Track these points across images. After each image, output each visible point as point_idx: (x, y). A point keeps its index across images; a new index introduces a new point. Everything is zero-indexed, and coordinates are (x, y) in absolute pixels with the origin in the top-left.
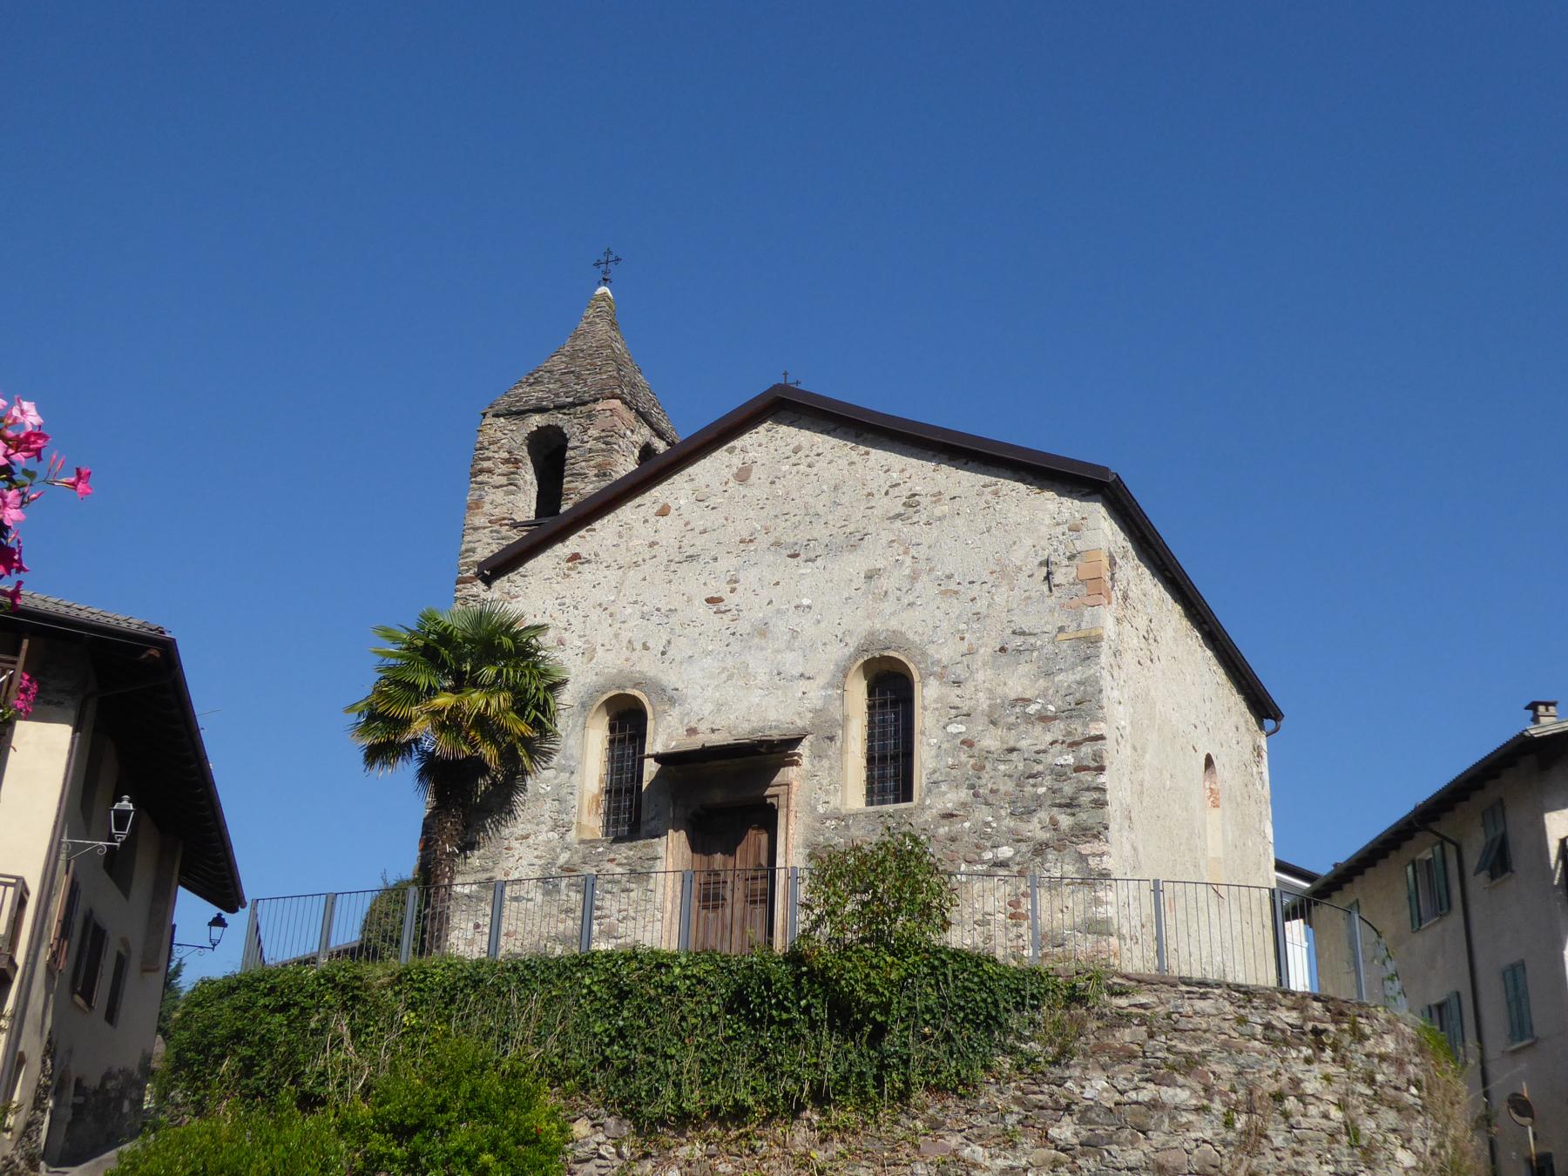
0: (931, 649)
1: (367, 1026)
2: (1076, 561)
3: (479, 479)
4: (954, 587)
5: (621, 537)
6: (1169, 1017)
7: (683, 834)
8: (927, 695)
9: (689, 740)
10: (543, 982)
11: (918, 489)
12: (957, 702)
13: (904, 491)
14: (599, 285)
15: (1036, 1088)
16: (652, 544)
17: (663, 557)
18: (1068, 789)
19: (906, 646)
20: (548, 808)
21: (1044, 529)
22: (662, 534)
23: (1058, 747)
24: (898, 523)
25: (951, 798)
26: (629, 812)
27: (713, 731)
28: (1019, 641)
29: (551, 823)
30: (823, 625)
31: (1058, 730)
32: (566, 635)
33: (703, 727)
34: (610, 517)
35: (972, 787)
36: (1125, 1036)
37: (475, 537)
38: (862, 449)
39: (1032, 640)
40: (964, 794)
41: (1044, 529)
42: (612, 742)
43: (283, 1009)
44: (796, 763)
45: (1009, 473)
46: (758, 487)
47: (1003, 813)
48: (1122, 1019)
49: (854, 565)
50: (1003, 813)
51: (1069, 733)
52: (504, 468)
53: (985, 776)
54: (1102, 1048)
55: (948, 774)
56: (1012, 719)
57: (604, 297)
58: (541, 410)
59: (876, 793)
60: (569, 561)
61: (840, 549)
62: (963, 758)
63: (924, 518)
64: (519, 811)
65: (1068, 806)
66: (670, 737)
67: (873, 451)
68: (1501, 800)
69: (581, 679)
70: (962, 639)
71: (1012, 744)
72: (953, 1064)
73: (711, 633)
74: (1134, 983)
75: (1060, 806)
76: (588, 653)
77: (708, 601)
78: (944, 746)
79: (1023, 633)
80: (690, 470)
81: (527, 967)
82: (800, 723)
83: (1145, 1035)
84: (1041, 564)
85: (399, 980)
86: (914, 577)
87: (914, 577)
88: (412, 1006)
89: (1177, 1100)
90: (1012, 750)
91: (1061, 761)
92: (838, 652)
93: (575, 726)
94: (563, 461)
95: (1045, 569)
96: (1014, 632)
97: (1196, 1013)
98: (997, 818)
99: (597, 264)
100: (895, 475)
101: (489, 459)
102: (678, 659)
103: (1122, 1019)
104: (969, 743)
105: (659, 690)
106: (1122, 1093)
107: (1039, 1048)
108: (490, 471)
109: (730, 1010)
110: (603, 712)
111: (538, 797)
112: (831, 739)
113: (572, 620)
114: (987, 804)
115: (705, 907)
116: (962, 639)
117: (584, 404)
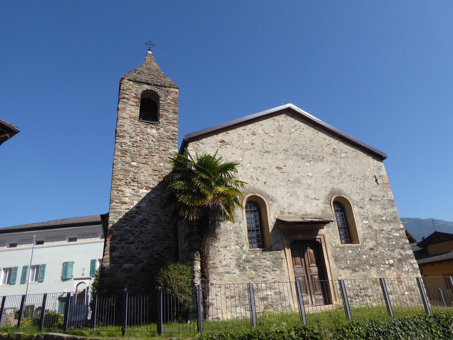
0: (352, 197)
2: (382, 178)
3: (124, 100)
11: (335, 147)
16: (252, 144)
24: (332, 156)
25: (371, 244)
27: (289, 213)
30: (317, 183)
33: (286, 211)
34: (234, 130)
52: (134, 100)
61: (317, 161)
62: (370, 231)
66: (275, 214)
67: (319, 132)
71: (381, 228)
77: (276, 167)
78: (364, 227)
80: (260, 122)
98: (386, 251)
99: (146, 44)
101: (127, 94)
102: (271, 186)
111: (227, 231)
117: (166, 87)
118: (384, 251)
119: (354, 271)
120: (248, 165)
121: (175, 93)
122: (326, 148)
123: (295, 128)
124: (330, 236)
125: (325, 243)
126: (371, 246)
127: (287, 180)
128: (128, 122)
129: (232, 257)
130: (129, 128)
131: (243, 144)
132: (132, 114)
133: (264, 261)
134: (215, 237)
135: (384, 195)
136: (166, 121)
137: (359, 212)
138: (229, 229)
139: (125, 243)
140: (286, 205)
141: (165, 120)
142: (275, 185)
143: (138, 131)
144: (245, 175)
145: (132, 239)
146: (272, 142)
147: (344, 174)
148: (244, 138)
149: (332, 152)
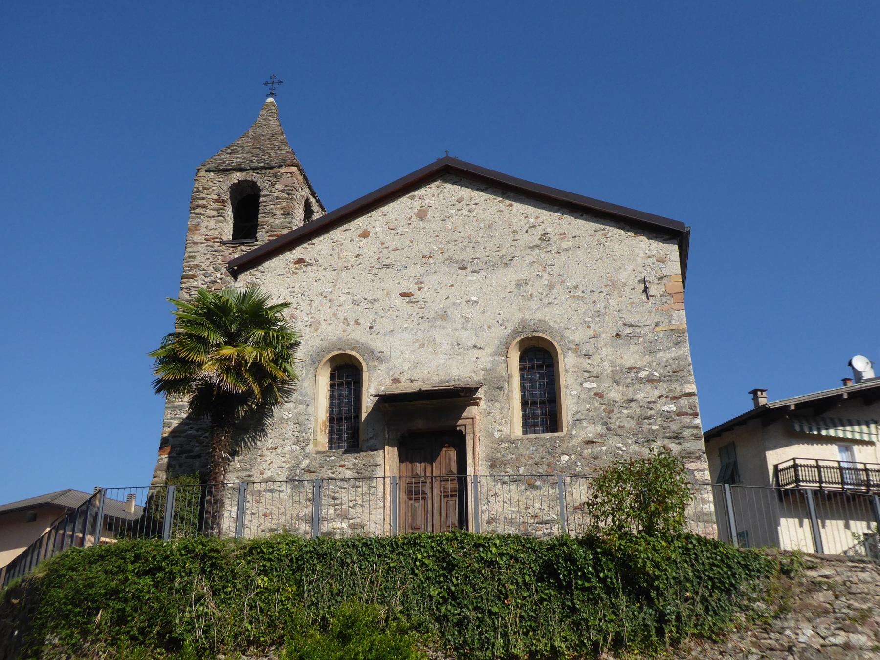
0: (567, 333)
1: (225, 587)
2: (664, 281)
3: (197, 211)
4: (579, 293)
5: (334, 249)
6: (845, 585)
7: (396, 449)
8: (568, 364)
9: (394, 386)
10: (379, 556)
11: (549, 230)
12: (589, 368)
13: (540, 231)
14: (268, 96)
15: (766, 635)
17: (366, 264)
18: (674, 427)
19: (551, 331)
20: (290, 428)
21: (639, 260)
22: (365, 249)
23: (663, 400)
24: (537, 251)
25: (591, 431)
26: (349, 430)
27: (412, 381)
28: (628, 330)
29: (293, 439)
31: (662, 388)
32: (297, 313)
33: (404, 378)
35: (605, 423)
36: (821, 597)
37: (195, 248)
38: (507, 202)
39: (638, 330)
40: (600, 428)
41: (639, 260)
42: (332, 386)
43: (151, 572)
44: (477, 404)
45: (613, 223)
46: (433, 223)
47: (629, 441)
48: (815, 586)
49: (507, 277)
50: (629, 441)
51: (671, 391)
52: (215, 206)
53: (614, 417)
54: (807, 607)
55: (587, 415)
56: (629, 380)
57: (272, 104)
58: (240, 170)
59: (529, 425)
60: (295, 263)
61: (496, 266)
62: (597, 404)
63: (555, 249)
64: (268, 430)
65: (675, 438)
68: (734, 443)
69: (310, 343)
70: (589, 327)
71: (630, 396)
72: (710, 618)
73: (405, 316)
74: (818, 561)
75: (670, 438)
76: (315, 325)
77: (401, 294)
78: (582, 396)
79: (631, 325)
80: (383, 209)
81: (365, 544)
82: (476, 378)
83: (833, 598)
84: (639, 282)
85: (251, 552)
86: (551, 286)
87: (551, 286)
88: (265, 572)
89: (861, 643)
90: (632, 400)
91: (666, 408)
92: (501, 333)
93: (307, 374)
94: (257, 203)
95: (643, 286)
96: (625, 325)
97: (860, 581)
98: (626, 445)
99: (266, 84)
100: (532, 220)
101: (203, 199)
102: (382, 331)
103: (815, 586)
104: (599, 395)
105: (371, 353)
106: (824, 638)
107: (764, 606)
108: (204, 207)
109: (540, 579)
110: (328, 365)
111: (282, 421)
112: (500, 389)
113: (301, 303)
114: (617, 435)
115: (411, 499)
116: (589, 327)
117: (272, 168)
118: (621, 445)
119: (531, 486)
120: (343, 298)
121: (289, 175)
122: (526, 235)
123: (458, 206)
124: (495, 423)
125: (473, 433)
126: (590, 435)
127: (418, 316)
128: (202, 248)
129: (283, 465)
130: (203, 259)
131: (340, 258)
132: (210, 233)
133: (341, 469)
134: (263, 430)
135: (662, 320)
136: (268, 234)
137: (576, 366)
138: (285, 417)
139: (187, 457)
140: (407, 366)
141: (268, 232)
142: (391, 329)
143: (219, 262)
144: (333, 318)
145: (197, 450)
146: (399, 245)
147: (558, 287)
148: (344, 246)
149: (539, 243)
